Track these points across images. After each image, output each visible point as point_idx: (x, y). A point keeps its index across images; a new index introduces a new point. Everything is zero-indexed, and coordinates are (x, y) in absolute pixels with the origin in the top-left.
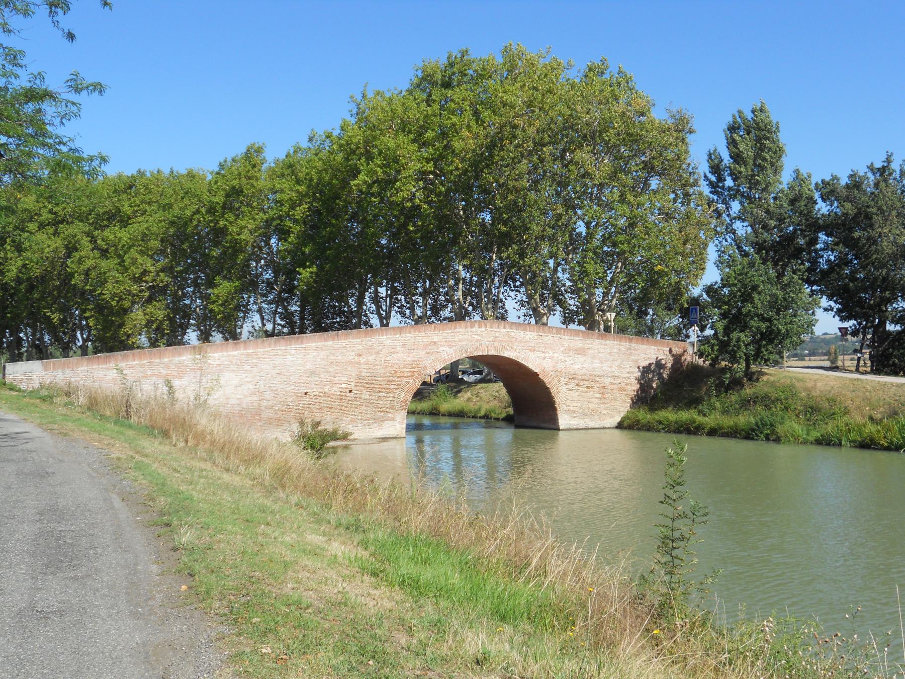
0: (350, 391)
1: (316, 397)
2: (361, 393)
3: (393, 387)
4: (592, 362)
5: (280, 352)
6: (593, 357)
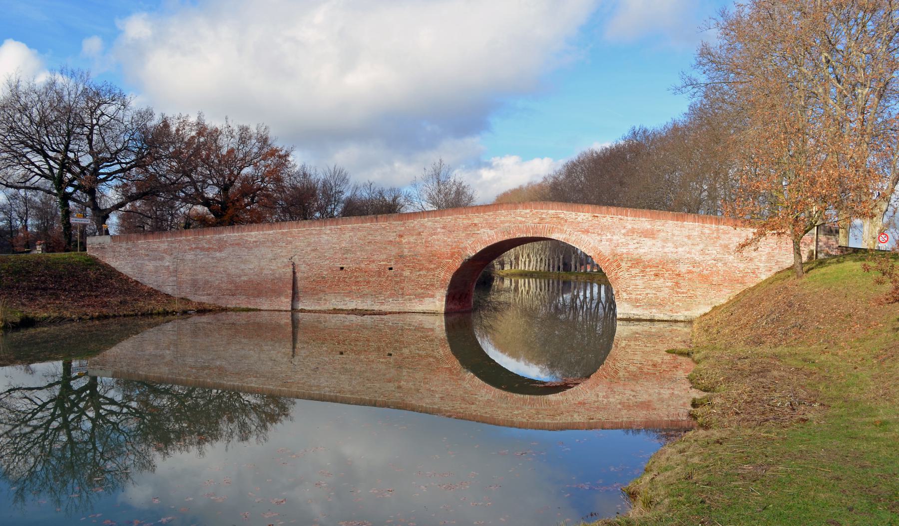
0: (391, 269)
1: (352, 271)
2: (403, 270)
3: (432, 266)
4: (663, 247)
5: (314, 232)
6: (665, 240)
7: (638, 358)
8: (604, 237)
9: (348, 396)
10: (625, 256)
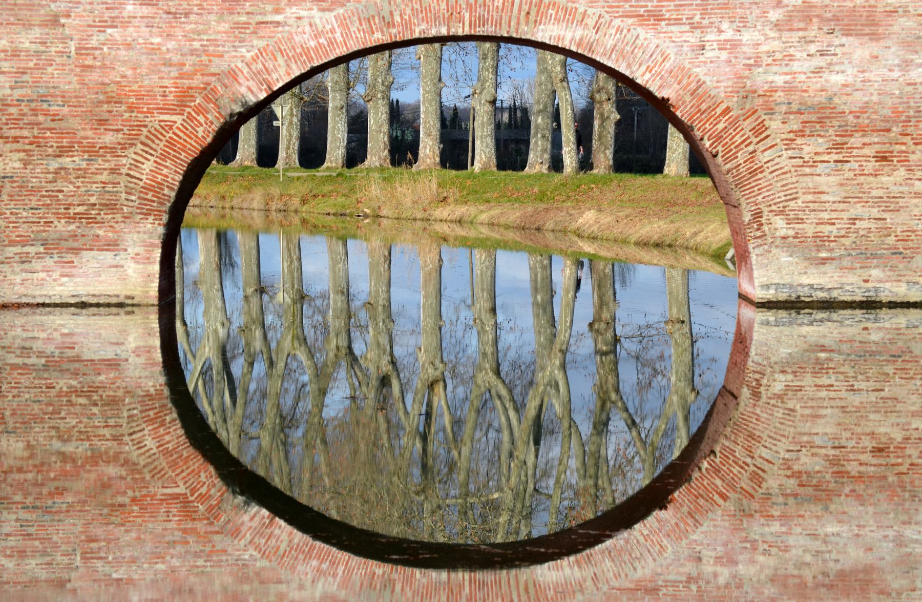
3: (109, 139)
4: (906, 65)
7: (825, 428)
8: (711, 36)
9: (485, 231)
10: (779, 96)
